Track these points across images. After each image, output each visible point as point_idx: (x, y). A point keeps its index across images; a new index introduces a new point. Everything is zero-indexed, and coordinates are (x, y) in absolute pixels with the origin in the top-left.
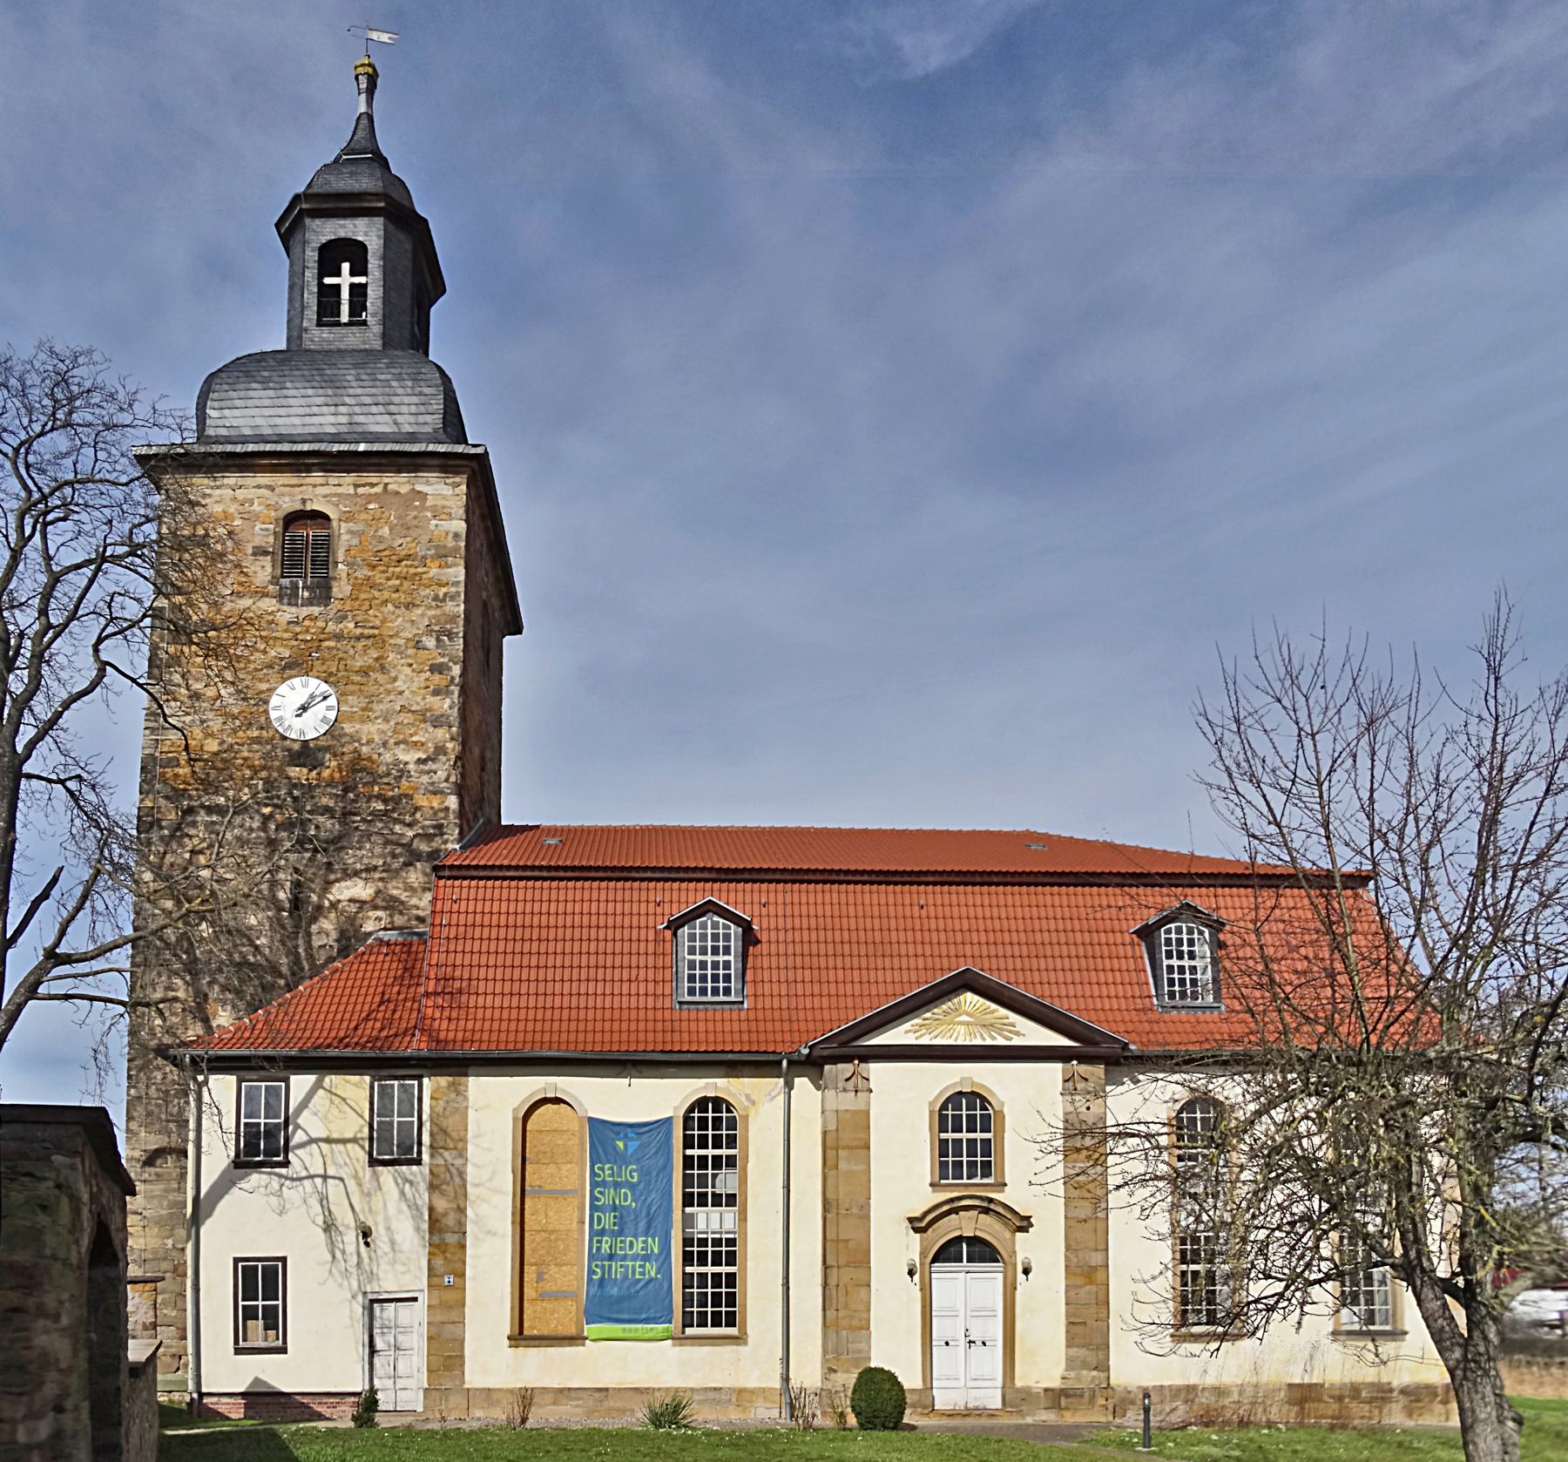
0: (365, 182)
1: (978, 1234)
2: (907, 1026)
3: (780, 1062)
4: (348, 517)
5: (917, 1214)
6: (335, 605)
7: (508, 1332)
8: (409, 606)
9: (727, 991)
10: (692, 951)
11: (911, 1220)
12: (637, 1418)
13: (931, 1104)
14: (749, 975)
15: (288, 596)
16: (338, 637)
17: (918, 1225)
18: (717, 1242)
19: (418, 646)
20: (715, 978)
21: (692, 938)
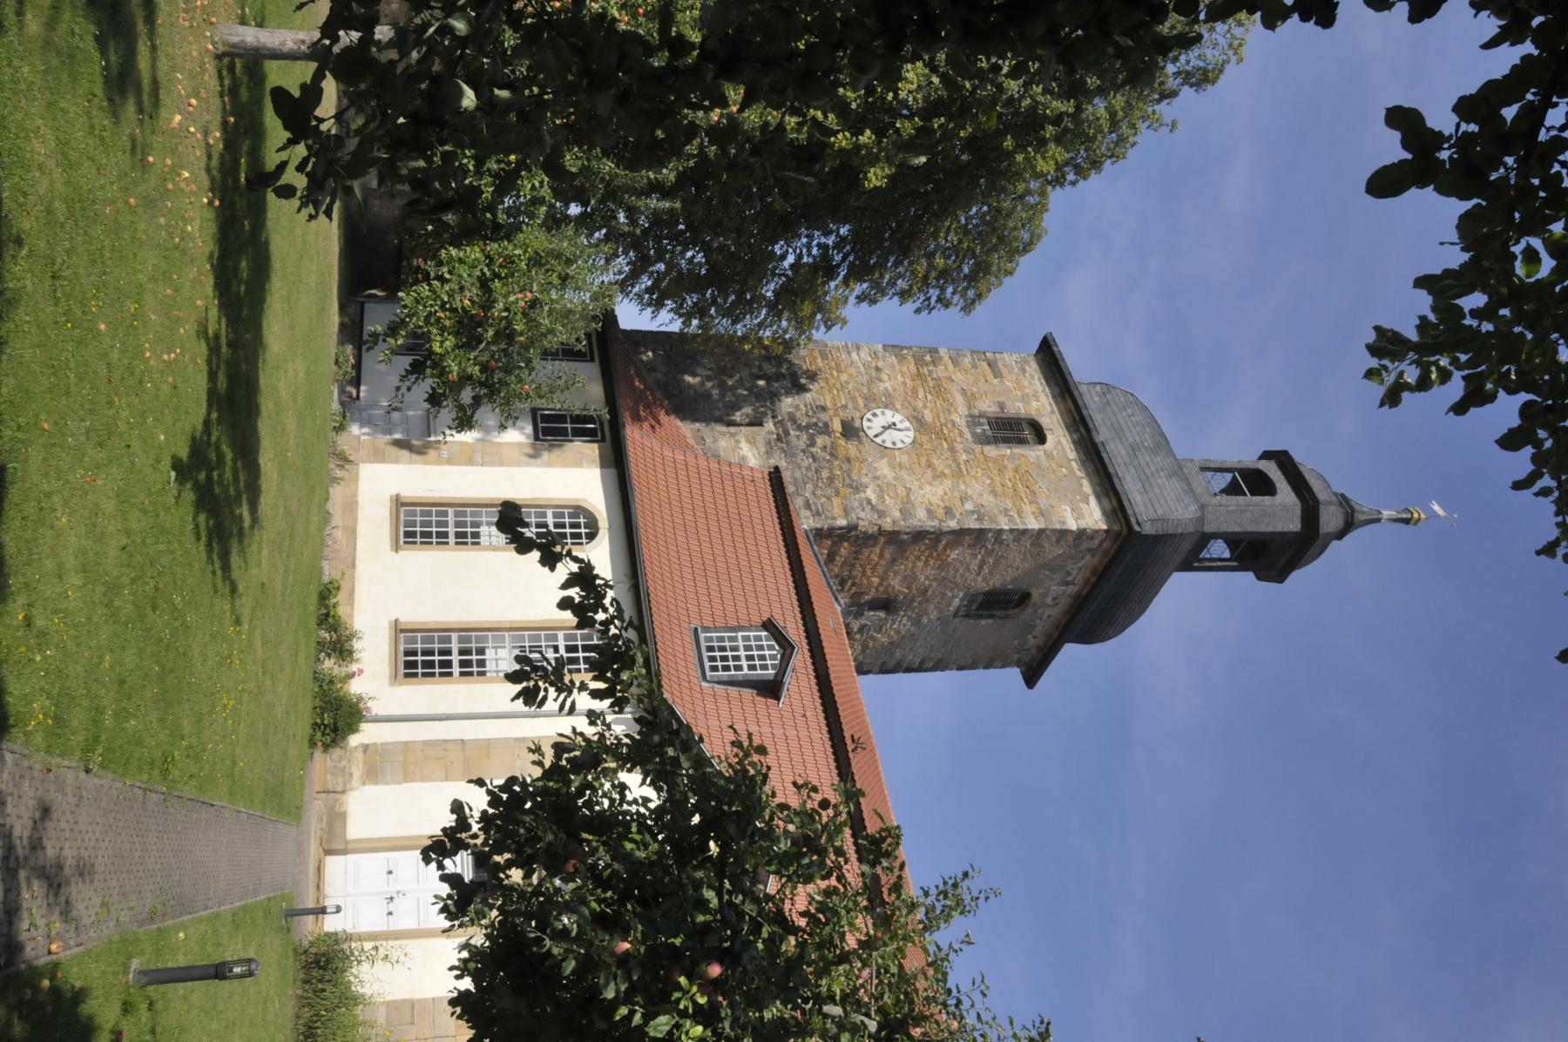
0: (1330, 519)
4: (1049, 456)
6: (978, 448)
8: (994, 492)
9: (714, 669)
10: (746, 639)
12: (329, 571)
14: (733, 690)
15: (973, 420)
16: (952, 449)
18: (482, 663)
19: (964, 499)
20: (724, 659)
21: (758, 638)
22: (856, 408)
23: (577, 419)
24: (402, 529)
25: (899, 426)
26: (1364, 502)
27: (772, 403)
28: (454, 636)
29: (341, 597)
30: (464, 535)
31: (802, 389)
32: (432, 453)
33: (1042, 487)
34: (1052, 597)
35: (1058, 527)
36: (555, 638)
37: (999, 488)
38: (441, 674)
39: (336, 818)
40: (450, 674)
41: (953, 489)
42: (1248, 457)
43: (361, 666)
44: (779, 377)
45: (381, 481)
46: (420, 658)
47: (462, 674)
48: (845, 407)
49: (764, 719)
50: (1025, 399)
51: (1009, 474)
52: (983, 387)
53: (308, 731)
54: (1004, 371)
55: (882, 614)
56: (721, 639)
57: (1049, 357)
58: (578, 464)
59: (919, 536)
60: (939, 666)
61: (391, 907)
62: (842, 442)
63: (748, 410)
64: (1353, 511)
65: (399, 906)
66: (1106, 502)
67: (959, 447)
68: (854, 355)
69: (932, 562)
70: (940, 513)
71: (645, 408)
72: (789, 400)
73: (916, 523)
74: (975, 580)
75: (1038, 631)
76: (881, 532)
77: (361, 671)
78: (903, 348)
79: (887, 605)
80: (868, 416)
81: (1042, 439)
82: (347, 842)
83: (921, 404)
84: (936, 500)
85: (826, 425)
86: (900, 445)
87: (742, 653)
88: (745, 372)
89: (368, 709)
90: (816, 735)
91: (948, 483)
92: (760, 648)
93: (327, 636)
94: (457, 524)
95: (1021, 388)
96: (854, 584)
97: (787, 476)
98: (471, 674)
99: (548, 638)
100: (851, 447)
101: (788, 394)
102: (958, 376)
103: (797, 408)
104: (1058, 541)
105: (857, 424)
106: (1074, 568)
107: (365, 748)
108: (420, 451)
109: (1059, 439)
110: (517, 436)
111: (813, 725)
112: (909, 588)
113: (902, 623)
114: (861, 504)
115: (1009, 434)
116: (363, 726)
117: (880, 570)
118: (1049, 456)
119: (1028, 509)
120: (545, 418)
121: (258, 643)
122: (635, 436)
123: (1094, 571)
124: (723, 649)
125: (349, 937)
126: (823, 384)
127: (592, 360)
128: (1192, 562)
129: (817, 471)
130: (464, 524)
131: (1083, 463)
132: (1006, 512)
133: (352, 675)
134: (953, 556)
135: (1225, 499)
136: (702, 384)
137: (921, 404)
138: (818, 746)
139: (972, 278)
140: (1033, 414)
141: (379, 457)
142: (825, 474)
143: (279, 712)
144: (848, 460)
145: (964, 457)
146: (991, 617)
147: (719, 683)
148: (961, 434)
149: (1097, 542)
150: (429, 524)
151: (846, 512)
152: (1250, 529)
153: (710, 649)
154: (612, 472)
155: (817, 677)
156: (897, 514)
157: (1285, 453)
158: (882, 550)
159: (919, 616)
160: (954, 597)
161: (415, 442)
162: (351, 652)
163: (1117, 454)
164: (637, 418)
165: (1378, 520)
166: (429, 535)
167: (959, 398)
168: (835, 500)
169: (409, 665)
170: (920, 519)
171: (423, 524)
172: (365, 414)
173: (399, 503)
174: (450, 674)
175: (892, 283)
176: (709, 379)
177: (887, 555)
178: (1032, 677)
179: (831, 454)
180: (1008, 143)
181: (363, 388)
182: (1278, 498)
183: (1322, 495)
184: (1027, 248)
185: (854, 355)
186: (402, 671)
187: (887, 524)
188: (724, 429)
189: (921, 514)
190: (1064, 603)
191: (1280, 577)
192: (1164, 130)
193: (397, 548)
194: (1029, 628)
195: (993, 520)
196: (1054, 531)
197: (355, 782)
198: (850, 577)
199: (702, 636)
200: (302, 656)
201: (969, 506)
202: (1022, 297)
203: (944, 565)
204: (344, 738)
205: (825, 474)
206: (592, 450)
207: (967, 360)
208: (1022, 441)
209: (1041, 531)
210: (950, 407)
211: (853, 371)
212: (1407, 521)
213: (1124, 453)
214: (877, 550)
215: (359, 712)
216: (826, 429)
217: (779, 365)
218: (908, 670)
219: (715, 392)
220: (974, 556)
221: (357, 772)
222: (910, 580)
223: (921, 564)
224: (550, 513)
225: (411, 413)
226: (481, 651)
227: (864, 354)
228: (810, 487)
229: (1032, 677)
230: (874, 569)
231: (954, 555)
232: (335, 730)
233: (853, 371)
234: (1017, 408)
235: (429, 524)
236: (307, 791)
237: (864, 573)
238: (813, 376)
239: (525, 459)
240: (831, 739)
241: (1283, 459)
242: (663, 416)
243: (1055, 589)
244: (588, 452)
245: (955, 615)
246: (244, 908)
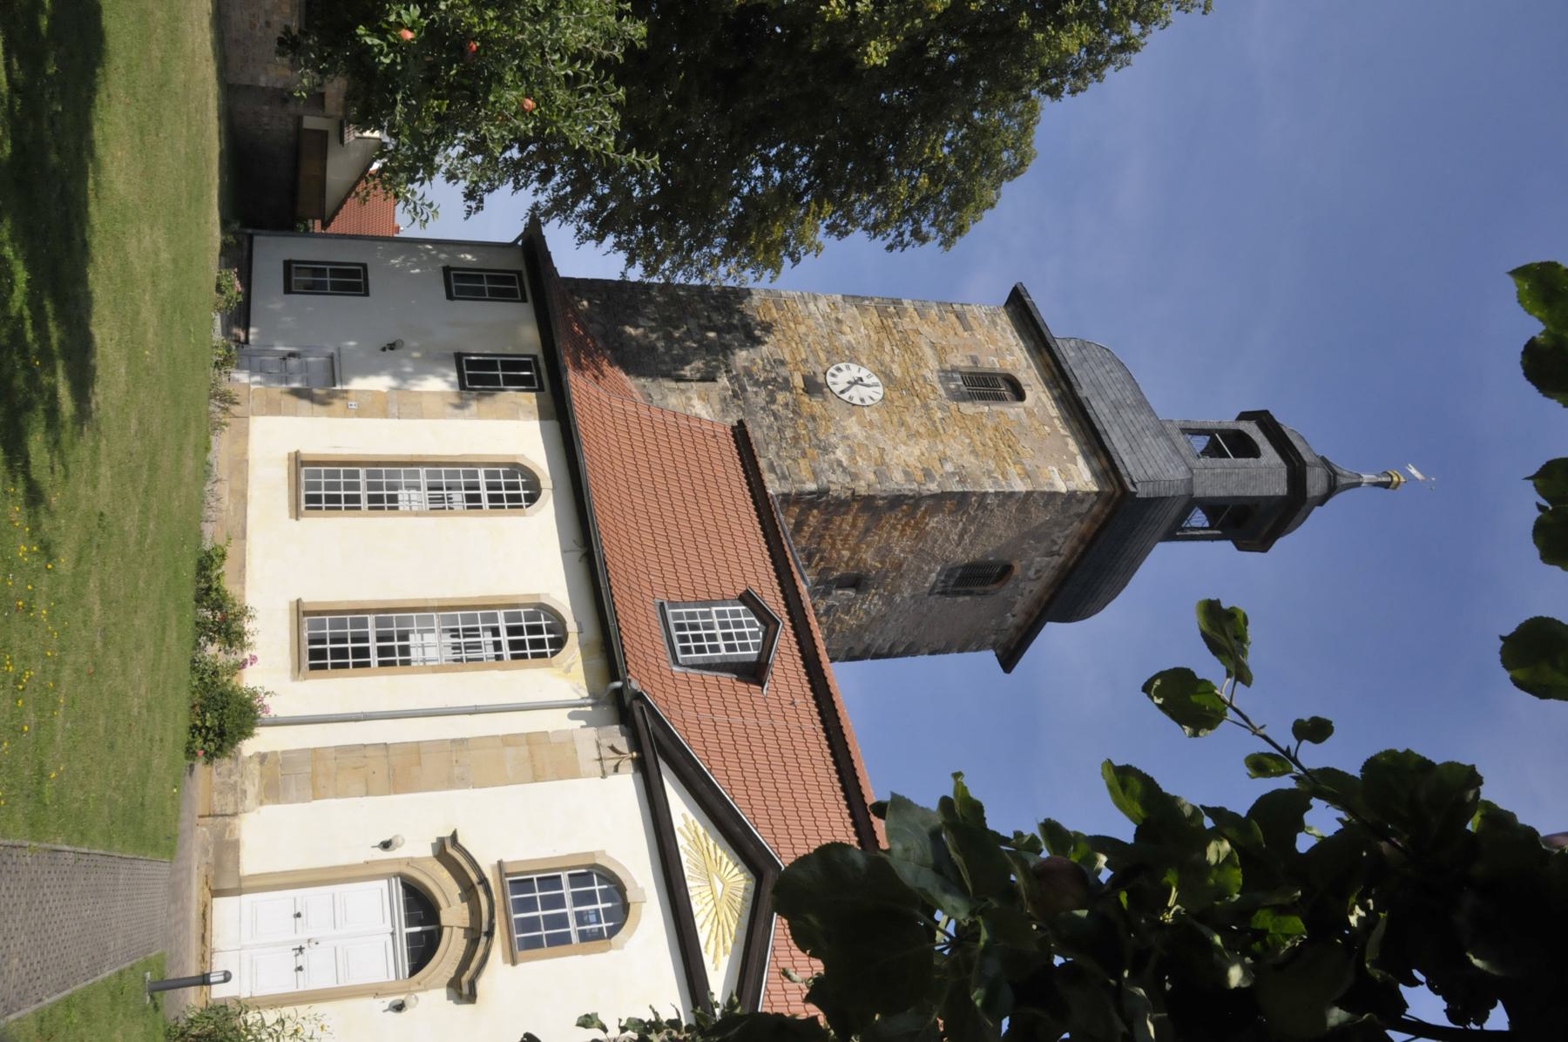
0: (1316, 482)
1: (446, 931)
2: (691, 817)
3: (618, 679)
4: (1030, 413)
5: (461, 840)
6: (953, 405)
7: (303, 451)
8: (974, 452)
9: (686, 650)
11: (454, 837)
12: (211, 535)
13: (603, 852)
15: (946, 375)
16: (926, 406)
17: (448, 851)
18: (405, 650)
20: (697, 638)
21: (736, 614)
22: (818, 362)
23: (507, 366)
24: (303, 493)
25: (866, 381)
26: (1345, 469)
27: (725, 356)
28: (371, 618)
29: (227, 567)
30: (379, 499)
31: (757, 342)
32: (338, 404)
33: (1025, 447)
34: (1036, 569)
35: (1046, 489)
36: (494, 618)
37: (980, 448)
38: (356, 665)
39: (226, 849)
40: (367, 665)
41: (930, 449)
42: (1226, 418)
43: (254, 653)
44: (730, 328)
45: (275, 437)
46: (328, 646)
47: (382, 664)
48: (805, 361)
49: (747, 709)
50: (998, 352)
51: (989, 433)
52: (953, 341)
53: (185, 736)
54: (974, 324)
55: (851, 593)
56: (692, 616)
57: (1019, 307)
58: (513, 415)
59: (896, 501)
60: (910, 651)
61: (301, 960)
62: (806, 399)
63: (699, 364)
64: (1336, 474)
65: (310, 958)
66: (1095, 463)
67: (933, 404)
68: (811, 306)
69: (908, 531)
70: (919, 475)
71: (587, 358)
72: (744, 353)
73: (893, 486)
74: (955, 553)
75: (1018, 608)
77: (254, 659)
78: (863, 299)
79: (857, 582)
80: (832, 370)
81: (1020, 395)
82: (240, 879)
83: (887, 358)
84: (912, 461)
85: (786, 380)
86: (868, 402)
87: (718, 631)
88: (693, 324)
89: (264, 707)
90: (807, 725)
91: (924, 443)
92: (738, 625)
93: (209, 614)
94: (371, 486)
95: (994, 342)
96: (821, 559)
97: (756, 434)
98: (393, 663)
99: (485, 618)
100: (814, 405)
101: (742, 346)
102: (926, 329)
103: (753, 361)
104: (1045, 506)
105: (820, 379)
106: (1060, 537)
107: (262, 758)
108: (324, 401)
109: (1038, 395)
110: (440, 384)
111: (804, 715)
112: (883, 562)
113: (873, 602)
114: (831, 467)
115: (983, 390)
116: (257, 730)
117: (852, 541)
118: (1030, 413)
119: (1013, 470)
120: (471, 365)
121: (94, 601)
122: (579, 384)
123: (1082, 540)
124: (694, 627)
125: (244, 1006)
126: (779, 336)
127: (524, 300)
128: (1176, 533)
129: (779, 430)
130: (379, 486)
131: (1066, 421)
132: (989, 474)
133: (243, 665)
134: (932, 524)
135: (1208, 461)
136: (645, 336)
137: (887, 358)
138: (811, 739)
139: (957, 204)
140: (1009, 369)
141: (273, 409)
142: (789, 433)
143: (135, 704)
144: (813, 418)
145: (939, 415)
146: (969, 593)
147: (692, 667)
148: (934, 390)
149: (1086, 506)
150: (336, 486)
151: (815, 475)
152: (1235, 493)
153: (680, 627)
154: (553, 425)
155: (803, 658)
156: (872, 477)
157: (1266, 412)
158: (854, 519)
159: (892, 594)
160: (930, 571)
161: (317, 391)
162: (241, 635)
163: (1100, 410)
164: (578, 366)
165: (1358, 485)
166: (337, 499)
167: (928, 352)
168: (802, 462)
169: (315, 654)
170: (897, 481)
171: (329, 486)
172: (255, 361)
173: (299, 462)
174: (367, 665)
175: (865, 212)
176: (652, 330)
177: (861, 524)
178: (1008, 661)
179: (794, 412)
180: (1024, 20)
181: (252, 330)
182: (1263, 460)
183: (1307, 457)
184: (1013, 173)
185: (811, 306)
186: (306, 661)
187: (862, 489)
188: (673, 385)
190: (1048, 575)
191: (1264, 545)
192: (1197, 12)
193: (297, 514)
194: (1009, 605)
195: (976, 482)
196: (1043, 493)
197: (250, 801)
199: (670, 612)
200: (172, 635)
201: (949, 467)
202: (1013, 229)
203: (921, 535)
204: (233, 745)
205: (789, 433)
206: (529, 400)
207: (934, 312)
208: (999, 398)
209: (1029, 494)
210: (920, 362)
211: (811, 322)
212: (1386, 485)
213: (1106, 411)
214: (850, 518)
215: (253, 710)
216: (786, 385)
217: (730, 315)
219: (661, 345)
220: (955, 523)
221: (252, 789)
222: (883, 552)
223: (896, 534)
224: (481, 472)
225: (311, 359)
226: (404, 636)
227: (822, 304)
228: (773, 448)
229: (1008, 661)
230: (845, 541)
231: (933, 523)
232: (221, 734)
233: (811, 322)
234: (991, 363)
235: (336, 486)
236: (184, 815)
237: (833, 545)
238: (768, 328)
239: (450, 410)
240: (825, 730)
241: (1264, 419)
242: (605, 366)
243: (1039, 561)
244: (524, 402)
246: (68, 1003)
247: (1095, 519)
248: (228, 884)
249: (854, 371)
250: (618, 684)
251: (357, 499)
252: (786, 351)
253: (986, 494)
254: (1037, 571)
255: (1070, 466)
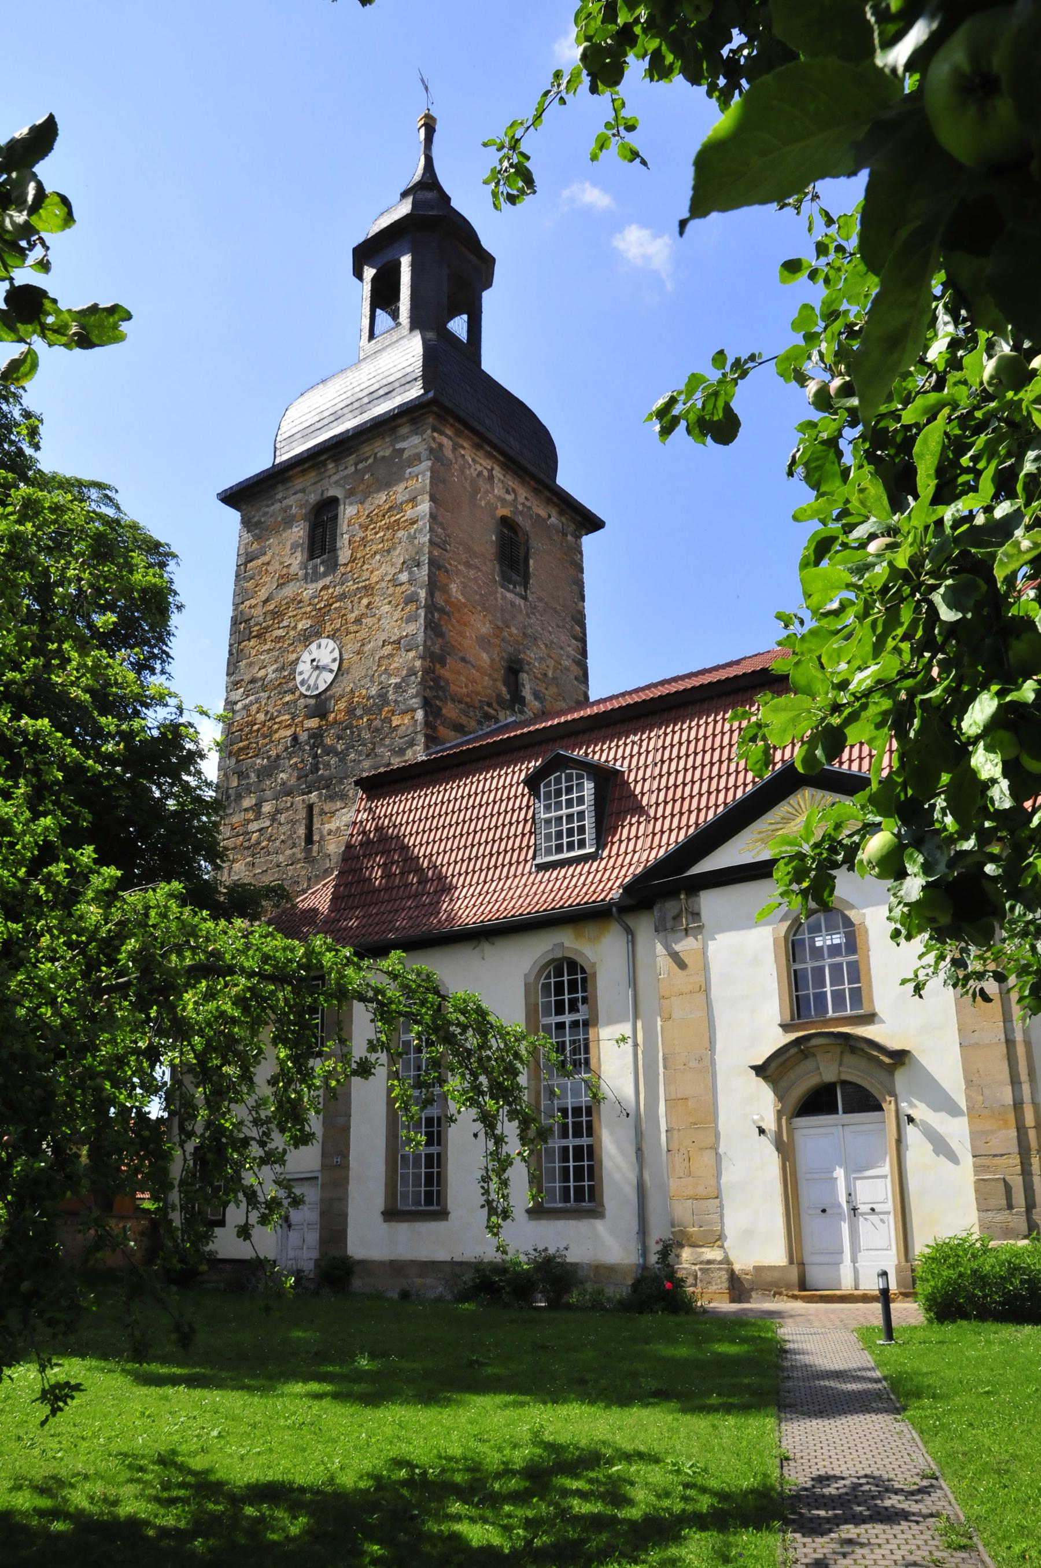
1: (844, 1077)
5: (760, 1062)
16: (342, 597)
34: (502, 494)
55: (524, 676)
59: (433, 628)
60: (580, 619)
67: (338, 590)
76: (427, 672)
80: (303, 689)
96: (489, 705)
123: (478, 447)
148: (325, 588)
156: (412, 654)
157: (356, 251)
160: (504, 598)
170: (416, 629)
173: (392, 1214)
178: (592, 523)
189: (411, 628)
190: (511, 483)
191: (487, 262)
198: (481, 708)
209: (433, 499)
216: (317, 736)
218: (584, 653)
221: (713, 1254)
222: (483, 642)
226: (564, 1111)
229: (592, 523)
245: (525, 598)
247: (458, 433)
248: (794, 1275)
249: (304, 667)
250: (614, 909)
251: (429, 1157)
252: (283, 733)
253: (430, 541)
254: (508, 492)
255: (406, 455)
